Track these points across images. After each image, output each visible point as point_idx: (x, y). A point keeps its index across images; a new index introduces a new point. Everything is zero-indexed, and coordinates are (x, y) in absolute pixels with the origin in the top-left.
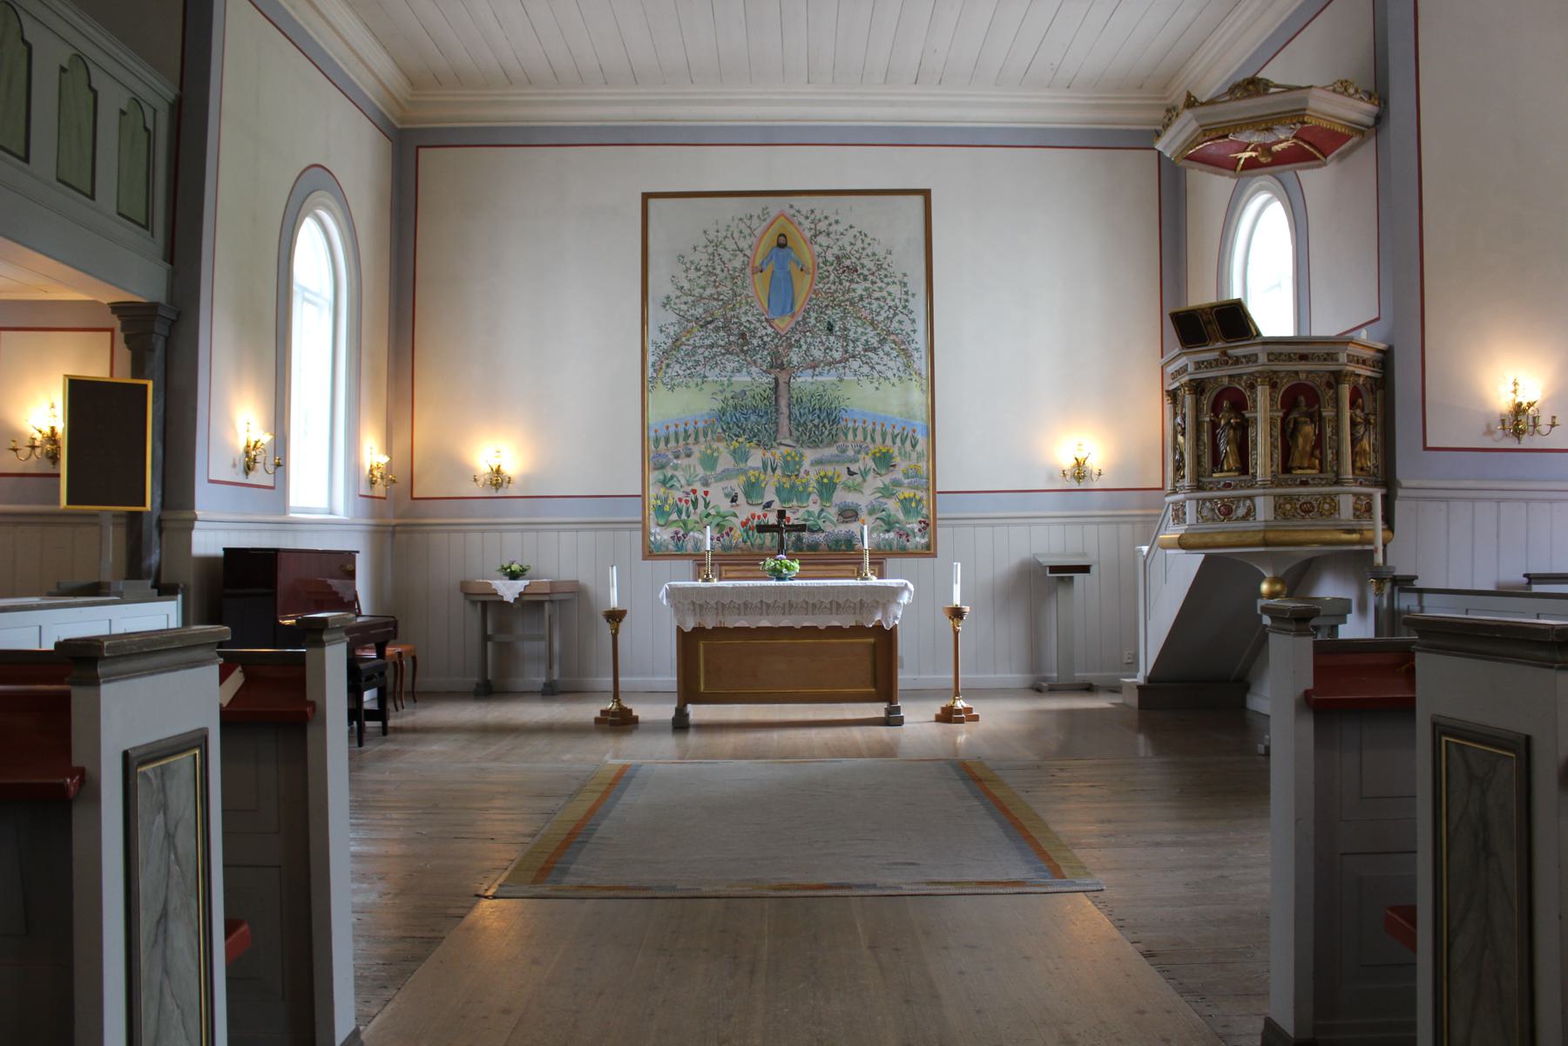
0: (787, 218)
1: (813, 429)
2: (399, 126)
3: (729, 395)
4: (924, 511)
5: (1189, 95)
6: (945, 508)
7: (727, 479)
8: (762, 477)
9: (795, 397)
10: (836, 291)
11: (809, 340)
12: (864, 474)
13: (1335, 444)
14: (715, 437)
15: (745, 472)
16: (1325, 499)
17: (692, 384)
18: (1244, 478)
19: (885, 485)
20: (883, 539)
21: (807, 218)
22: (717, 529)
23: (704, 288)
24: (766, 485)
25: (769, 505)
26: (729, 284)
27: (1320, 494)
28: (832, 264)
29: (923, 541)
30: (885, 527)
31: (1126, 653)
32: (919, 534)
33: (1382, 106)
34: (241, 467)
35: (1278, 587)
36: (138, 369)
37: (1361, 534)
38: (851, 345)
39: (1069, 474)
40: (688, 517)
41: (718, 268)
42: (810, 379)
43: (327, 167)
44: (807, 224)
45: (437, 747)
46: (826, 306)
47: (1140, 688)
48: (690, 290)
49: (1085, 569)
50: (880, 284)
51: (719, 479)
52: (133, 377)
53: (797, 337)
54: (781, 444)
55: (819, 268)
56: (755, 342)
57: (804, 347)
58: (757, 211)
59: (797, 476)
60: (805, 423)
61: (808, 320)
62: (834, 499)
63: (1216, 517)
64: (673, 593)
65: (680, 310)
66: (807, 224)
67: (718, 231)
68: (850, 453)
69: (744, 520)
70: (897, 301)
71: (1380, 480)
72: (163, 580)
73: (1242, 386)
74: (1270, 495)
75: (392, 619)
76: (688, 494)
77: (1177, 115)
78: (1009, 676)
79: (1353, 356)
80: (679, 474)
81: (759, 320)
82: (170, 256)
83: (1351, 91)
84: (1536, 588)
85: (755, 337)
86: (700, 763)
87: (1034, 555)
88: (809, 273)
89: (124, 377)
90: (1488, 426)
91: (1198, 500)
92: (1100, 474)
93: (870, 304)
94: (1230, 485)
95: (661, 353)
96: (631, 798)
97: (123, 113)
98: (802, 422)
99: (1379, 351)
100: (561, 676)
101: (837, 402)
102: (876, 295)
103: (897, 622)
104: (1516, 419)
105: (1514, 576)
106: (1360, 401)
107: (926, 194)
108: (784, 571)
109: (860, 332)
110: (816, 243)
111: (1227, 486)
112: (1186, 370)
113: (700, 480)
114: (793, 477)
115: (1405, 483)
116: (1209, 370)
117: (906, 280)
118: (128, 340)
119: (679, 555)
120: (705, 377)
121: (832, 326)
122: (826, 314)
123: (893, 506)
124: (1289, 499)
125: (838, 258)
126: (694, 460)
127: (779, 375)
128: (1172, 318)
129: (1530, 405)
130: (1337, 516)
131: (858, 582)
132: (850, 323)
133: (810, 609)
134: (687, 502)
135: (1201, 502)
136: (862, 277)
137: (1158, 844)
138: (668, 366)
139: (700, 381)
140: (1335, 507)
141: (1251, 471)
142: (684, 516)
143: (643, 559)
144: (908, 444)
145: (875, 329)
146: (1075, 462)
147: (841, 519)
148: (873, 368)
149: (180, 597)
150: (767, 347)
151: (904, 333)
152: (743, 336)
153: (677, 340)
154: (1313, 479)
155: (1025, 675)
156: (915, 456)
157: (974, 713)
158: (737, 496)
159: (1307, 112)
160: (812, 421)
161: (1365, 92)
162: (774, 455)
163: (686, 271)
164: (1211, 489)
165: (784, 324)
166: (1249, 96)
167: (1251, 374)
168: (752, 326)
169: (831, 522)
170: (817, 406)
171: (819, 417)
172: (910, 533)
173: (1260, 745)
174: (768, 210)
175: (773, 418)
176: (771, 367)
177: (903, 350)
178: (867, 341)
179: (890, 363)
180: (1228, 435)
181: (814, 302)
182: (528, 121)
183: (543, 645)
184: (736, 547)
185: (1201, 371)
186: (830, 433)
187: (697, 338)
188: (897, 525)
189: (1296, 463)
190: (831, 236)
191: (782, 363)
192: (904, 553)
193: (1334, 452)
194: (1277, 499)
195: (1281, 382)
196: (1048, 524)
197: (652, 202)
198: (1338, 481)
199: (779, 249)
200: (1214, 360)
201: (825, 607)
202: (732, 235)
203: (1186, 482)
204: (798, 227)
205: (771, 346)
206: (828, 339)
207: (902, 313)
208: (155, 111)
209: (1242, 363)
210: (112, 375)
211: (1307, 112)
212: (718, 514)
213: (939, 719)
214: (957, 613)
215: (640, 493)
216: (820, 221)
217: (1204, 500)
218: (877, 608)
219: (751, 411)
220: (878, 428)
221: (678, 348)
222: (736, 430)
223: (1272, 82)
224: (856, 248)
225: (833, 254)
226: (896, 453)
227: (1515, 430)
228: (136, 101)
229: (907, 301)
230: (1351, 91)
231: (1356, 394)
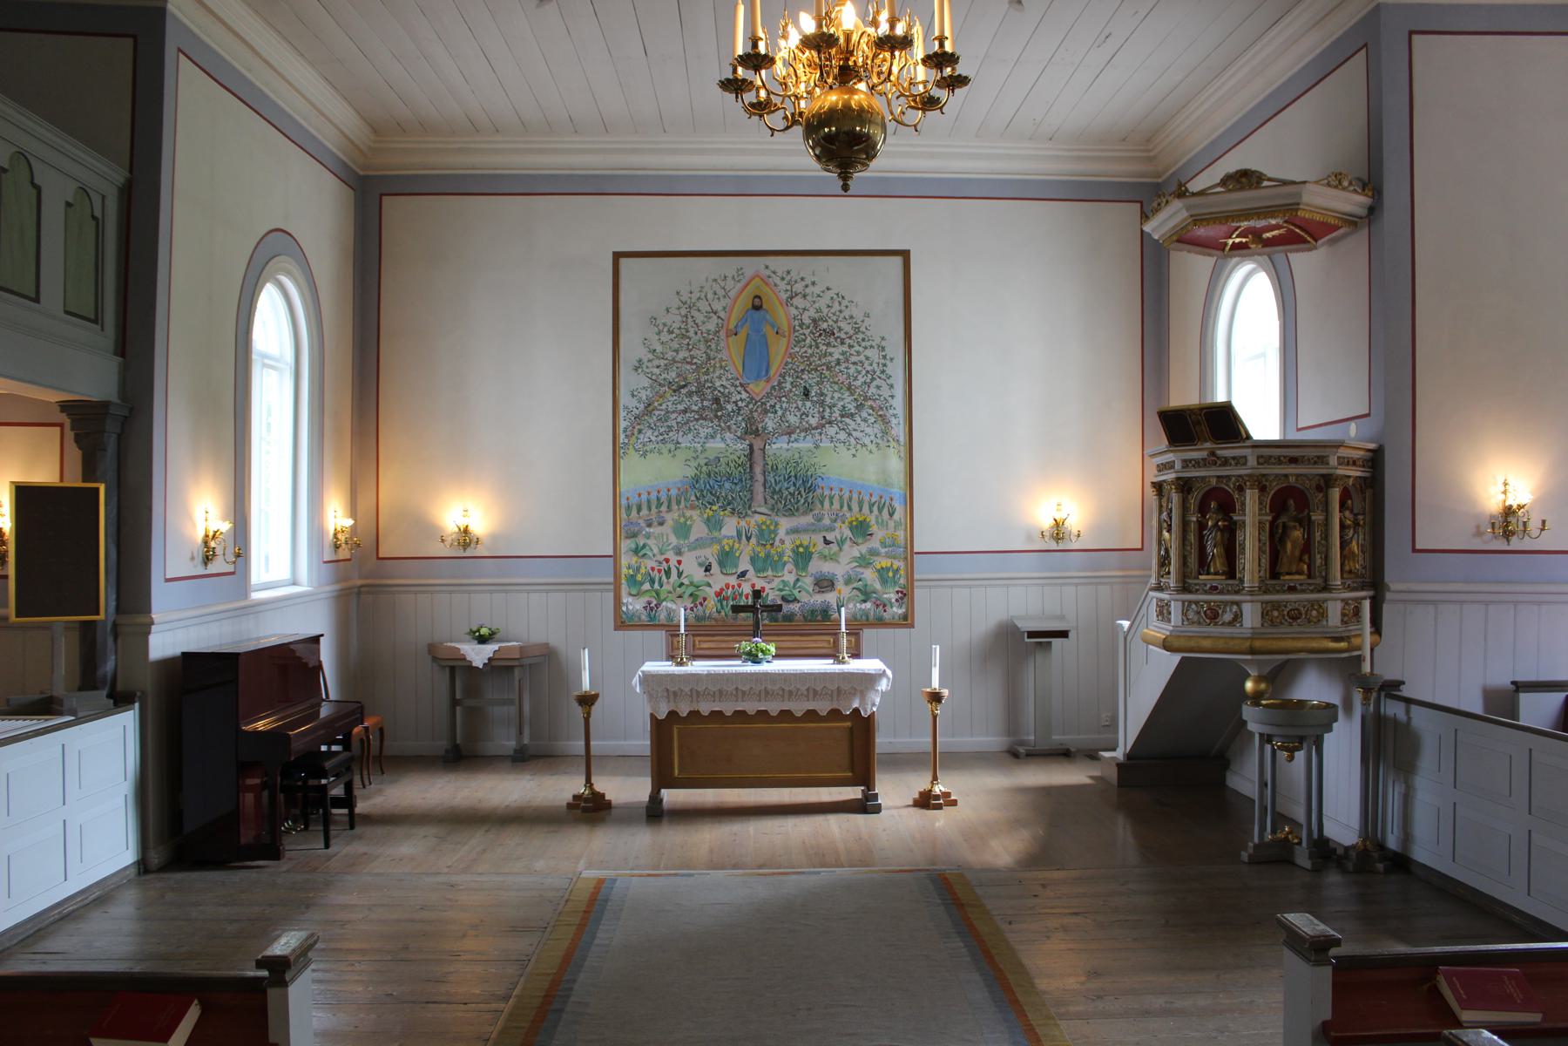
0: (762, 279)
1: (789, 497)
2: (361, 173)
3: (703, 462)
6: (922, 569)
7: (701, 548)
8: (737, 546)
9: (770, 463)
10: (812, 355)
11: (784, 405)
12: (841, 543)
13: (1324, 549)
14: (688, 506)
15: (719, 541)
16: (1312, 606)
17: (665, 451)
18: (1230, 582)
19: (861, 554)
21: (783, 279)
22: (691, 599)
23: (677, 351)
24: (741, 553)
25: (743, 574)
26: (702, 347)
27: (1308, 601)
28: (808, 327)
29: (900, 611)
30: (862, 598)
32: (897, 604)
33: (1376, 198)
34: (199, 559)
35: (1263, 686)
36: (89, 472)
37: (1349, 642)
38: (828, 410)
40: (661, 587)
41: (692, 331)
42: (785, 446)
43: (285, 229)
44: (782, 285)
45: (408, 848)
46: (803, 371)
47: (1119, 766)
48: (662, 353)
49: (1063, 634)
50: (857, 348)
51: (692, 548)
52: (84, 481)
54: (755, 512)
55: (795, 331)
56: (729, 407)
57: (780, 413)
58: (730, 272)
59: (772, 545)
60: (780, 490)
61: (784, 385)
62: (809, 568)
63: (1201, 620)
66: (782, 285)
67: (691, 293)
68: (827, 521)
69: (718, 590)
70: (875, 365)
71: (1367, 580)
74: (1257, 601)
75: (359, 705)
76: (660, 563)
77: (1167, 202)
78: (985, 739)
79: (1344, 458)
81: (733, 385)
82: (121, 349)
83: (1346, 184)
85: (729, 402)
86: (676, 875)
88: (785, 337)
89: (75, 481)
90: (1478, 527)
91: (1183, 602)
92: (1079, 536)
93: (847, 368)
94: (1216, 588)
95: (633, 418)
96: (609, 934)
97: (68, 205)
98: (777, 489)
100: (531, 739)
101: (813, 469)
102: (853, 359)
103: (875, 709)
104: (1506, 521)
106: (1350, 502)
107: (905, 255)
108: (760, 654)
109: (836, 398)
110: (792, 305)
111: (1214, 589)
112: (1173, 467)
113: (672, 549)
114: (768, 547)
115: (1393, 586)
117: (883, 344)
118: (78, 439)
120: (678, 443)
121: (808, 391)
122: (802, 379)
123: (869, 576)
124: (1277, 605)
125: (814, 321)
127: (754, 442)
129: (1520, 507)
130: (1325, 623)
131: (838, 668)
133: (786, 697)
134: (659, 571)
135: (1186, 604)
136: (839, 340)
137: (1146, 1013)
138: (640, 431)
139: (673, 448)
140: (1323, 613)
141: (1238, 575)
142: (656, 586)
143: (615, 630)
144: (885, 511)
145: (852, 394)
147: (817, 589)
148: (850, 434)
149: (137, 705)
150: (742, 412)
151: (882, 398)
152: (716, 400)
153: (649, 405)
154: (1301, 585)
155: (1005, 739)
156: (893, 524)
157: (953, 798)
158: (710, 566)
159: (1301, 207)
160: (787, 489)
161: (1359, 179)
163: (659, 333)
165: (759, 388)
166: (1242, 189)
167: (1240, 476)
168: (727, 390)
169: (808, 592)
170: (793, 474)
171: (794, 485)
172: (887, 603)
173: (1243, 853)
174: (743, 271)
175: (748, 486)
176: (746, 433)
177: (881, 416)
178: (844, 407)
179: (868, 430)
181: (790, 366)
182: (496, 169)
183: (513, 709)
188: (874, 595)
189: (1284, 569)
190: (807, 297)
191: (757, 429)
192: (880, 623)
193: (1323, 557)
194: (1264, 605)
195: (1270, 485)
196: (1026, 586)
197: (623, 262)
198: (1326, 588)
199: (754, 311)
200: (1202, 459)
201: (802, 695)
202: (706, 296)
203: (1172, 581)
204: (774, 288)
205: (745, 411)
206: (804, 405)
207: (880, 378)
208: (103, 197)
210: (62, 480)
211: (1301, 207)
212: (692, 583)
214: (936, 698)
215: (611, 553)
216: (796, 282)
217: (1190, 602)
218: (854, 694)
219: (724, 478)
220: (855, 496)
221: (651, 412)
222: (709, 497)
223: (1265, 175)
224: (833, 310)
225: (810, 317)
226: (873, 522)
227: (1505, 532)
228: (83, 190)
229: (885, 365)
230: (1346, 184)
231: (1345, 495)
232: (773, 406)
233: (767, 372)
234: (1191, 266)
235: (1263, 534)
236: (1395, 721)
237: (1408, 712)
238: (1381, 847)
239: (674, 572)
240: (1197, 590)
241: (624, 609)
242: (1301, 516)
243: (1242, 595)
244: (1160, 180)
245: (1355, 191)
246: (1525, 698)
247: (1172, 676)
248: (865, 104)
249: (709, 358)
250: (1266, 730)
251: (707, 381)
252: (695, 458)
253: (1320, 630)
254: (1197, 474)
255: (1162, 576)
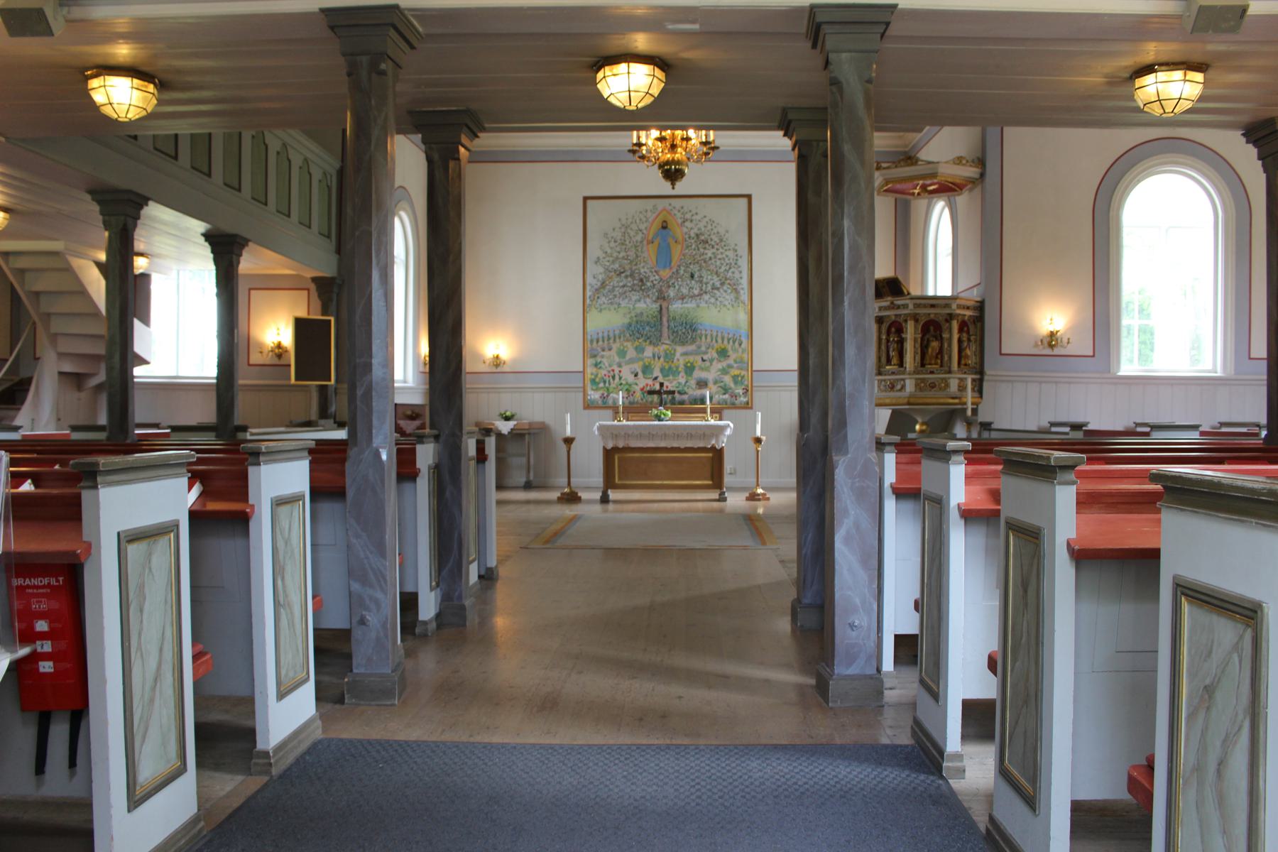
3: (633, 315)
4: (746, 383)
8: (652, 362)
10: (696, 254)
12: (711, 361)
15: (642, 360)
18: (901, 369)
20: (722, 399)
21: (679, 211)
23: (619, 252)
25: (656, 378)
26: (633, 249)
28: (693, 239)
30: (723, 392)
32: (743, 396)
35: (924, 427)
41: (627, 242)
42: (680, 306)
44: (679, 215)
46: (690, 263)
52: (323, 315)
53: (673, 281)
54: (663, 343)
55: (686, 241)
56: (649, 284)
57: (677, 287)
59: (673, 362)
64: (601, 428)
65: (605, 265)
68: (703, 349)
70: (731, 261)
72: (337, 420)
80: (605, 360)
81: (651, 272)
82: (339, 251)
83: (964, 162)
84: (1054, 429)
85: (648, 281)
88: (680, 244)
91: (916, 379)
99: (977, 302)
102: (719, 256)
103: (724, 445)
105: (1045, 424)
107: (749, 197)
111: (893, 373)
114: (670, 363)
117: (736, 248)
119: (605, 406)
123: (727, 380)
124: (923, 380)
126: (613, 352)
129: (1057, 332)
131: (704, 423)
132: (704, 273)
134: (609, 376)
138: (598, 298)
139: (616, 306)
142: (607, 385)
144: (737, 344)
147: (697, 386)
148: (717, 299)
152: (641, 280)
162: (659, 350)
163: (609, 242)
164: (885, 375)
166: (908, 165)
167: (905, 314)
169: (692, 388)
178: (713, 284)
179: (726, 296)
183: (524, 460)
184: (637, 403)
186: (691, 337)
187: (615, 281)
189: (928, 362)
192: (734, 406)
197: (589, 203)
198: (950, 372)
205: (658, 286)
206: (691, 283)
208: (331, 176)
210: (309, 314)
212: (627, 383)
213: (748, 499)
214: (758, 441)
217: (882, 380)
220: (719, 334)
222: (637, 335)
230: (964, 162)
232: (673, 284)
233: (670, 264)
234: (919, 204)
239: (617, 377)
241: (589, 398)
244: (907, 149)
245: (971, 166)
248: (680, 159)
249: (637, 256)
251: (636, 269)
252: (630, 313)
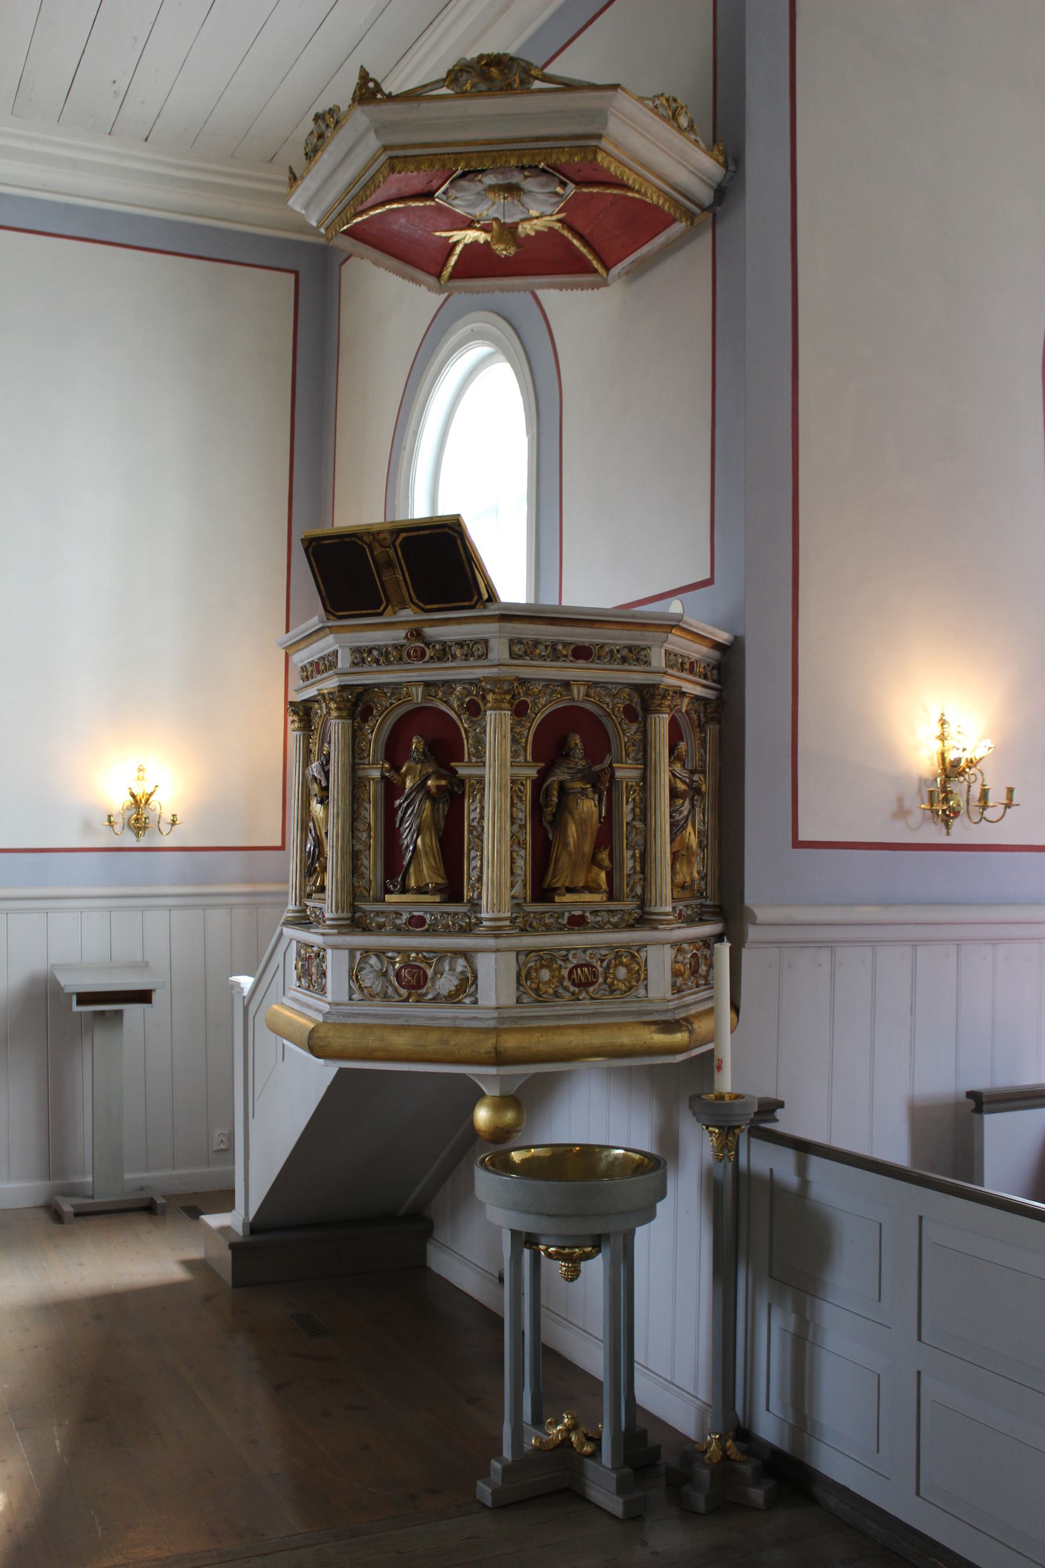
5: (364, 77)
13: (639, 839)
16: (618, 956)
18: (452, 908)
27: (611, 947)
31: (217, 1133)
33: (731, 168)
37: (691, 1032)
39: (118, 820)
49: (143, 997)
63: (390, 991)
71: (708, 902)
73: (453, 709)
83: (684, 121)
87: (52, 965)
90: (900, 800)
91: (352, 951)
92: (174, 823)
94: (421, 921)
99: (717, 646)
111: (417, 923)
112: (333, 665)
115: (762, 914)
116: (384, 668)
124: (547, 958)
128: (306, 550)
129: (971, 763)
130: (642, 992)
140: (638, 972)
141: (467, 894)
146: (131, 799)
154: (594, 913)
166: (491, 92)
167: (471, 682)
180: (420, 810)
185: (365, 668)
189: (562, 880)
194: (522, 958)
195: (535, 704)
196: (81, 910)
198: (643, 920)
200: (395, 647)
203: (328, 906)
209: (454, 657)
217: (366, 952)
235: (519, 805)
236: (772, 1186)
237: (802, 1170)
238: (743, 1434)
240: (380, 926)
242: (597, 768)
243: (478, 936)
246: (993, 1123)
247: (330, 1088)
250: (527, 1224)
253: (634, 1007)
254: (384, 678)
255: (309, 896)
